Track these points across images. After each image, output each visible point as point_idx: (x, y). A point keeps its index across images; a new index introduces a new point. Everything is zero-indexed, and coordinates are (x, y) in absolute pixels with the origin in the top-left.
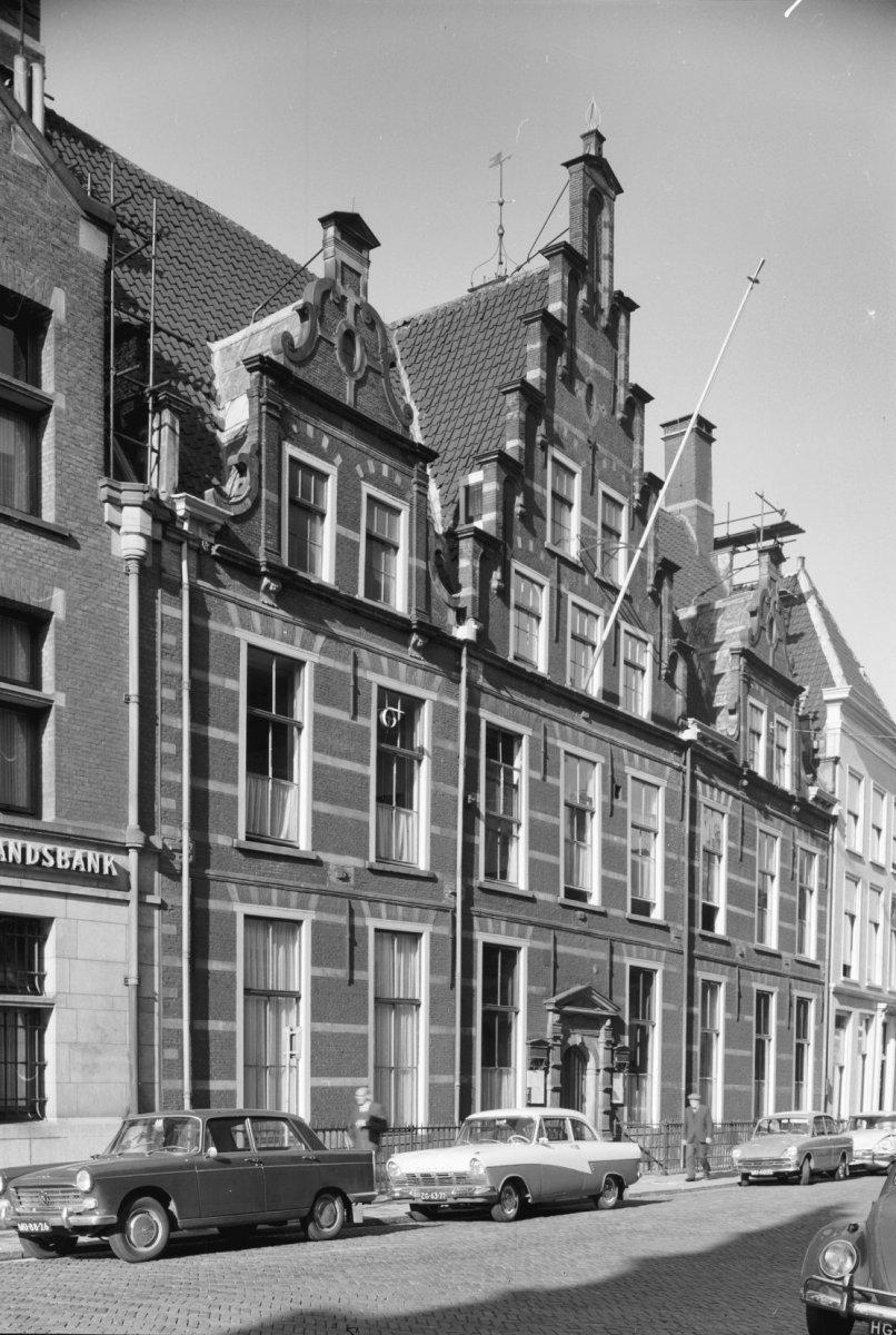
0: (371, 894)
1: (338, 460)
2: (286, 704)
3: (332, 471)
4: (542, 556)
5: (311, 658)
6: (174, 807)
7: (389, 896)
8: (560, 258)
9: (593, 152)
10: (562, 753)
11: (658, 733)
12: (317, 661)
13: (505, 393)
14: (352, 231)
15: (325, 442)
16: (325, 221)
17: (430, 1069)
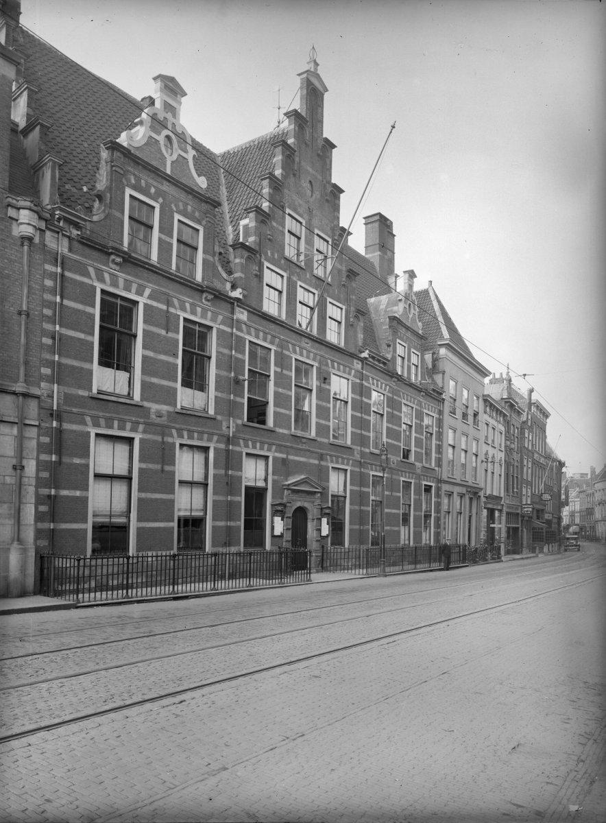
0: (177, 426)
1: (161, 200)
2: (202, 347)
3: (157, 206)
4: (283, 261)
5: (142, 301)
6: (50, 373)
7: (189, 427)
8: (293, 118)
9: (312, 70)
10: (294, 359)
11: (345, 354)
12: (145, 302)
13: (262, 180)
14: (171, 86)
15: (153, 190)
16: (155, 79)
17: (213, 517)
